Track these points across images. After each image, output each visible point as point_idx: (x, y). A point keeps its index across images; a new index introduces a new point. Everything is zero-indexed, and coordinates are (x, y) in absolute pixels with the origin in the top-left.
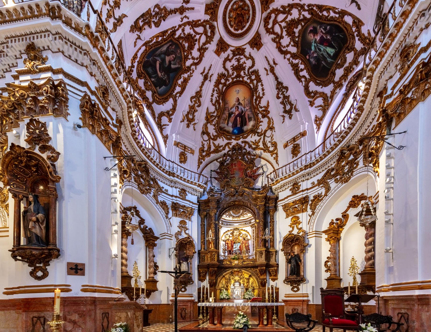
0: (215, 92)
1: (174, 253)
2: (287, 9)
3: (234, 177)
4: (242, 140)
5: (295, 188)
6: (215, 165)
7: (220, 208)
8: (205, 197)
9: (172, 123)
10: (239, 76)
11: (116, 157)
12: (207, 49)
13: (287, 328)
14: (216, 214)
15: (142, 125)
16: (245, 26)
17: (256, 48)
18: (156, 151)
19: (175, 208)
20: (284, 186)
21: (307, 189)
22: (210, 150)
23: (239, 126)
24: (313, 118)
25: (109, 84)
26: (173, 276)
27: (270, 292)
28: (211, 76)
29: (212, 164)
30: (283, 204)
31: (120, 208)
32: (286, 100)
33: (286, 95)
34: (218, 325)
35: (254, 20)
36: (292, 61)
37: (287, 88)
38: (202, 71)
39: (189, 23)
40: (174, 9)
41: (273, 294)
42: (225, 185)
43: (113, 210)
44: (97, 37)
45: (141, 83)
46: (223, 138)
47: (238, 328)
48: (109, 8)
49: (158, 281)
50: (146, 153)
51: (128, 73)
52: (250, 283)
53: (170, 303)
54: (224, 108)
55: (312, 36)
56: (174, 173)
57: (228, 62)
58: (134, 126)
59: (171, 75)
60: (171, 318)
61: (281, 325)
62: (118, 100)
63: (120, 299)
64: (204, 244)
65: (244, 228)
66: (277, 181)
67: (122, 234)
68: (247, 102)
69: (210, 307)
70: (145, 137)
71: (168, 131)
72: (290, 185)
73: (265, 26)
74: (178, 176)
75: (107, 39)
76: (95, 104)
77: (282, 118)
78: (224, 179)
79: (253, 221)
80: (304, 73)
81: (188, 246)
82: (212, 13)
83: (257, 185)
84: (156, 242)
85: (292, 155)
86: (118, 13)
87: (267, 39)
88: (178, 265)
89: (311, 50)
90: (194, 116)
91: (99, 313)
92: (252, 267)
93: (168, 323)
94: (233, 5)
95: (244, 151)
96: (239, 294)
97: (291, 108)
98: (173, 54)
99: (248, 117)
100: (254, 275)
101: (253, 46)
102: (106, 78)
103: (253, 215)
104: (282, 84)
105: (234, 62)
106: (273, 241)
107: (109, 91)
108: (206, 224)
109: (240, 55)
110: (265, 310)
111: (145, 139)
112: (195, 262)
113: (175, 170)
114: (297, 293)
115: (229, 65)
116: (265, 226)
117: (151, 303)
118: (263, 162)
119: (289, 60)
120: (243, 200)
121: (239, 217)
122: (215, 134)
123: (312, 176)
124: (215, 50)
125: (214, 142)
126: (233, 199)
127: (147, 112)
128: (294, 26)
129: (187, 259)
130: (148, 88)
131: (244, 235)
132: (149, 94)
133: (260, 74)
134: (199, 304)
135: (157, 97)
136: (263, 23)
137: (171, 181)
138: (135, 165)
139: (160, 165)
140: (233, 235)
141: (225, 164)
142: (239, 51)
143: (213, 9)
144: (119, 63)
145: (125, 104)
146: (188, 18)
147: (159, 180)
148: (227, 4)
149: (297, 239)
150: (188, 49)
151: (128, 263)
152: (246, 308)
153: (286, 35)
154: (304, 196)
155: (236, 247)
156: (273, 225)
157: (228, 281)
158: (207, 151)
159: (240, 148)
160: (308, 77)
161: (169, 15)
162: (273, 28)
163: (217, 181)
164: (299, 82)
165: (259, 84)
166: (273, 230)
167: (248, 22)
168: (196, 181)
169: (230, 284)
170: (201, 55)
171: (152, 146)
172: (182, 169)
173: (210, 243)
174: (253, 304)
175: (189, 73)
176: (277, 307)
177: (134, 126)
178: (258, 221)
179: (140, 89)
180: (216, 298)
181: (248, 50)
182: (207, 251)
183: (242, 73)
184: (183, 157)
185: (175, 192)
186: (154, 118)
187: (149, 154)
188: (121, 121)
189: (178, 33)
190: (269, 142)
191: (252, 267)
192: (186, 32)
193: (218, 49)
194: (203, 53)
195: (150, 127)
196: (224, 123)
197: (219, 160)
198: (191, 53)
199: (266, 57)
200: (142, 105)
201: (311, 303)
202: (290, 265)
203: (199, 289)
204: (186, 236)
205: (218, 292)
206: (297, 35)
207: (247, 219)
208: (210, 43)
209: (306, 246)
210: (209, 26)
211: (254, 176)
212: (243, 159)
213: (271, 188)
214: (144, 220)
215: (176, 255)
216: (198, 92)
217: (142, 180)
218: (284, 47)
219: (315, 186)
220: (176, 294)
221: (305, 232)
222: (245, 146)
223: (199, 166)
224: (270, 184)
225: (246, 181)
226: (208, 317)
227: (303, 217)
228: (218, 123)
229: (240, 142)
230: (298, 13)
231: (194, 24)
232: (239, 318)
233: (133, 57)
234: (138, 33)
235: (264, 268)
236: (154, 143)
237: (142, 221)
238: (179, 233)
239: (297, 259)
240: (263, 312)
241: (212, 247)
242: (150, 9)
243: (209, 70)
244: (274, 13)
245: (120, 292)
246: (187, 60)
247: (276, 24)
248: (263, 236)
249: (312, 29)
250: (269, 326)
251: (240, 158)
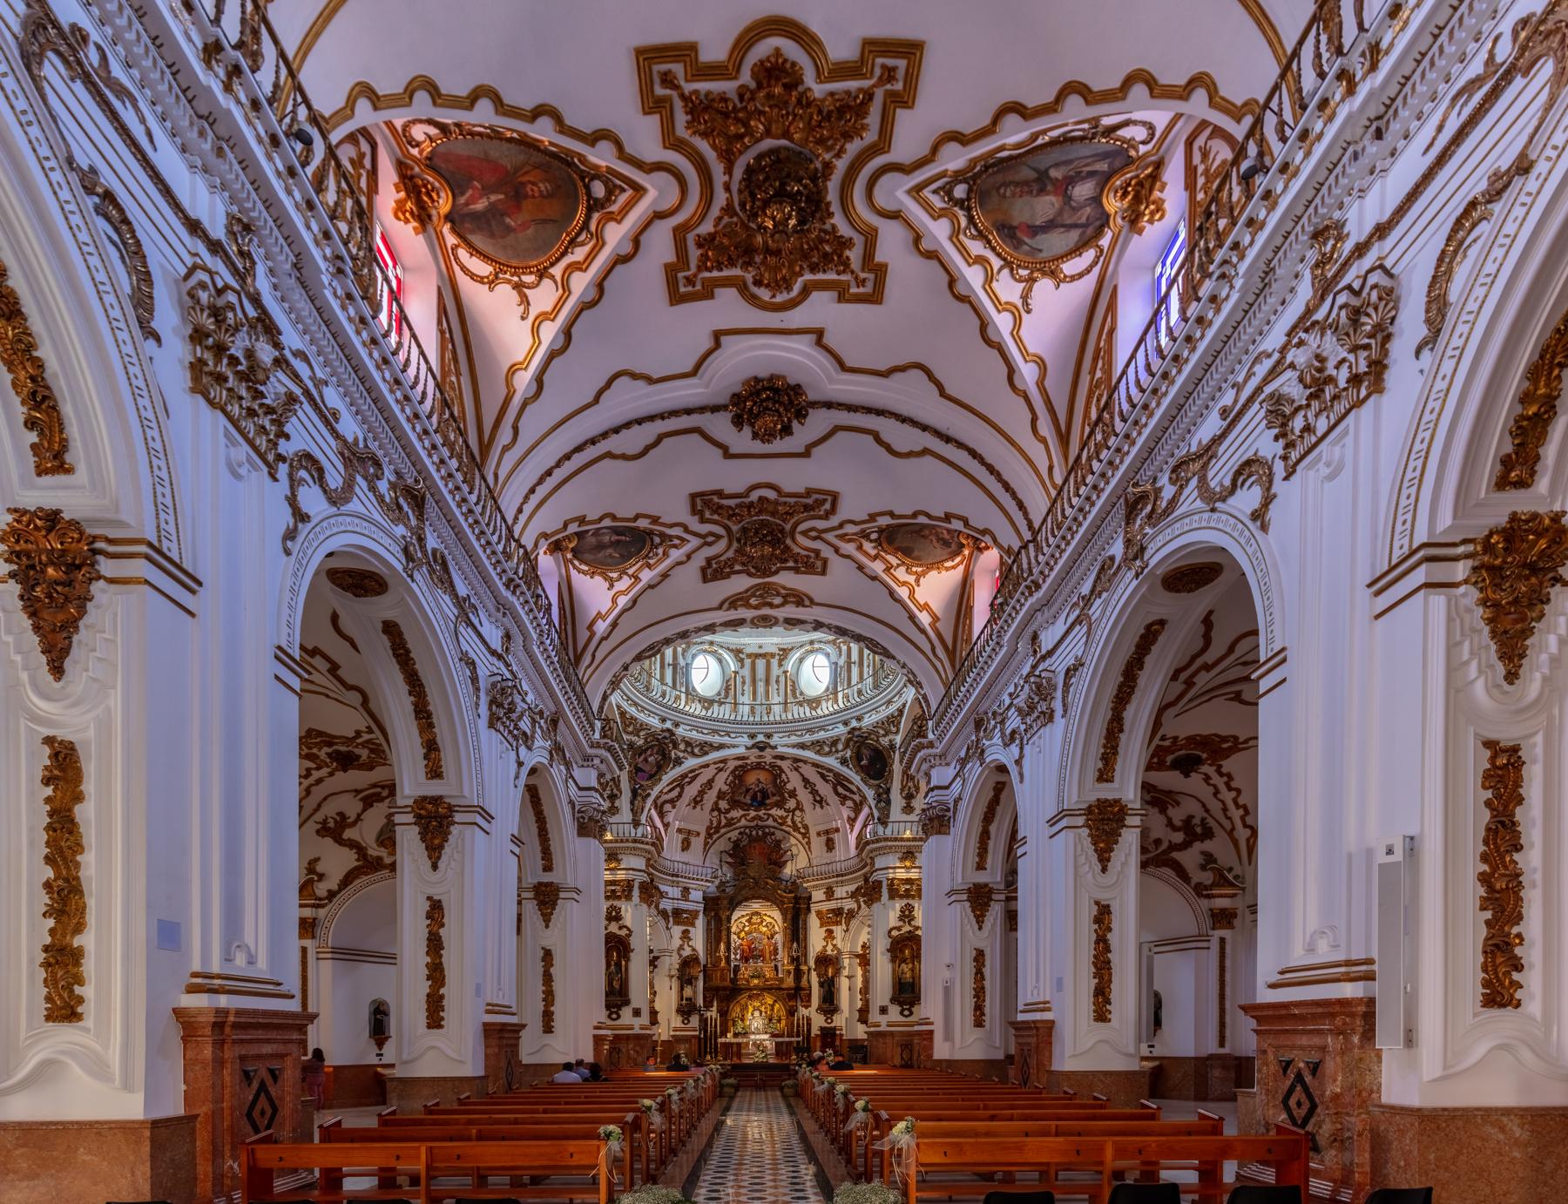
5: (830, 893)
71: (670, 818)
92: (774, 989)
118: (793, 841)
185: (674, 892)
191: (774, 989)
227: (838, 931)
238: (681, 948)
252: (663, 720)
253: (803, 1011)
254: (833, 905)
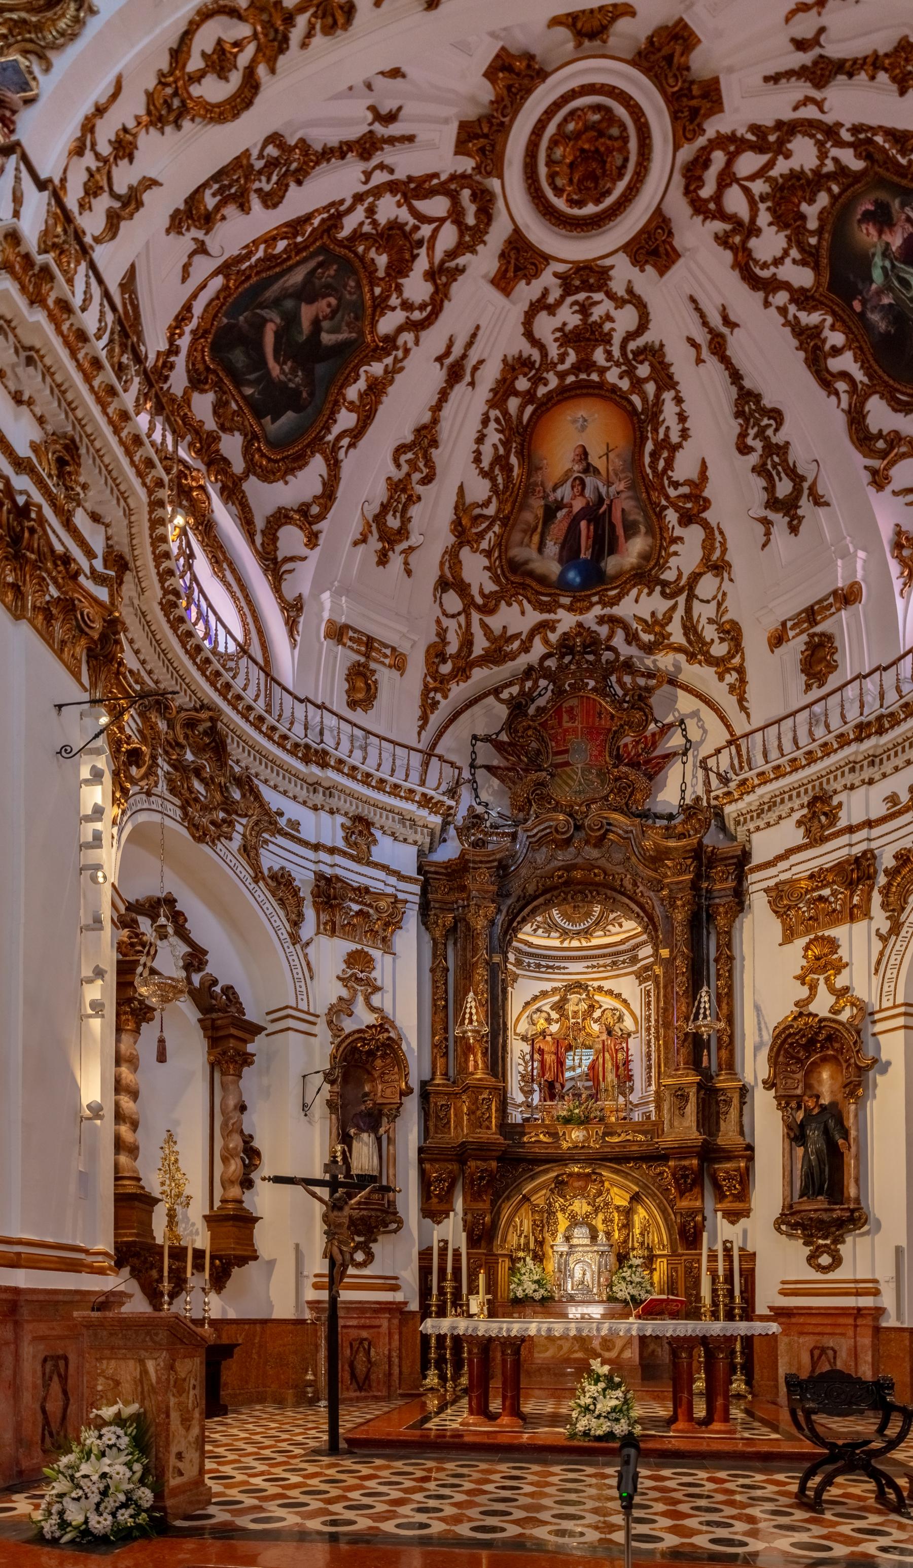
0: (493, 425)
1: (321, 1093)
2: (772, 138)
3: (567, 764)
4: (597, 610)
5: (820, 815)
6: (491, 716)
7: (508, 895)
8: (449, 851)
9: (318, 549)
10: (585, 364)
11: (100, 701)
12: (461, 270)
13: (790, 1438)
14: (492, 923)
15: (202, 566)
16: (609, 192)
17: (655, 266)
18: (256, 663)
19: (328, 897)
20: (772, 805)
21: (869, 824)
22: (470, 652)
23: (585, 555)
24: (886, 533)
25: (83, 427)
26: (320, 1200)
27: (721, 1272)
28: (475, 369)
29: (476, 709)
30: (771, 883)
31: (114, 905)
32: (776, 459)
33: (774, 440)
34: (505, 1420)
35: (646, 169)
36: (795, 317)
37: (777, 415)
38: (441, 350)
39: (392, 187)
40: (336, 145)
41: (729, 1278)
42: (531, 799)
43: (85, 919)
44: (45, 270)
45: (203, 406)
46: (520, 603)
47: (586, 1434)
48: (94, 164)
49: (257, 1219)
50: (218, 674)
51: (155, 378)
52: (637, 1231)
53: (308, 1315)
54: (527, 486)
55: (873, 231)
56: (325, 753)
57: (543, 316)
58: (170, 573)
59: (321, 369)
60: (310, 1384)
61: (765, 1423)
62: (114, 480)
63: (108, 1301)
64: (446, 1054)
65: (607, 985)
66: (743, 782)
67: (118, 1015)
68: (618, 463)
69: (472, 1339)
70: (215, 613)
71: (301, 581)
72: (796, 803)
73: (687, 192)
74: (341, 762)
75: (83, 267)
76: (28, 504)
77: (761, 529)
78: (526, 770)
79: (647, 950)
80: (846, 362)
81: (379, 1063)
82: (482, 150)
83: (661, 797)
84: (250, 1048)
85: (804, 677)
86: (124, 177)
87: (695, 236)
88: (339, 1148)
89: (872, 281)
90: (406, 521)
91: (31, 1354)
92: (636, 1156)
93: (297, 1404)
94: (565, 120)
95: (608, 655)
96: (588, 1277)
97: (797, 492)
98: (330, 295)
99: (624, 520)
100: (653, 1196)
101: (641, 258)
102: (71, 407)
103: (645, 928)
104: (757, 397)
105: (568, 317)
106: (729, 1042)
107: (83, 451)
108: (451, 964)
109: (591, 289)
110: (700, 1354)
111: (212, 619)
112: (409, 1134)
113: (329, 740)
114: (831, 1276)
115: (545, 326)
116: (697, 977)
117: (232, 1315)
118: (686, 703)
119: (783, 311)
120: (602, 862)
121: (587, 933)
122: (490, 587)
123: (888, 767)
124: (492, 275)
125: (488, 620)
126: (564, 857)
127: (223, 516)
128: (800, 193)
129: (374, 1119)
130: (227, 425)
131: (608, 1014)
132: (231, 446)
133: (668, 359)
134: (430, 1326)
135: (263, 455)
136: (678, 180)
137: (314, 786)
138: (171, 726)
139: (271, 720)
140: (563, 1014)
141: (531, 711)
142: (588, 277)
143: (486, 136)
144: (124, 346)
145: (142, 493)
146: (392, 171)
147: (266, 782)
148: (540, 121)
149: (830, 1038)
150: (388, 274)
151: (140, 1138)
152: (619, 1344)
153: (770, 224)
154: (857, 850)
155: (579, 1063)
156: (730, 971)
157: (544, 1221)
158: (458, 656)
159: (593, 644)
160: (859, 376)
161: (317, 163)
162: (718, 197)
163: (496, 782)
164: (824, 393)
165: (668, 396)
166: (730, 994)
167: (620, 176)
168: (412, 783)
169: (554, 1235)
170: (437, 291)
171: (238, 644)
172: (358, 733)
173: (470, 1050)
174: (651, 1327)
175: (389, 360)
176: (748, 1341)
177: (170, 573)
178: (665, 953)
179: (196, 430)
180: (495, 1296)
181: (623, 272)
182: (460, 1086)
183: (599, 356)
184: (360, 684)
185: (327, 829)
186: (250, 535)
187: (227, 676)
188: (121, 557)
189: (349, 224)
190: (710, 621)
191: (636, 1156)
192: (382, 218)
193: (506, 271)
194: (447, 285)
195: (234, 571)
196: (528, 546)
197: (505, 695)
198: (399, 289)
199: (693, 300)
200: (202, 488)
201: (890, 1322)
202: (800, 1151)
203: (425, 1255)
204: (370, 1019)
205: (503, 1266)
206: (812, 224)
207: (622, 942)
208: (474, 252)
209: (869, 1068)
210: (472, 200)
211: (647, 762)
212: (603, 690)
213: (719, 814)
214: (205, 953)
215: (329, 1103)
216: (424, 427)
217: (197, 785)
218: (765, 266)
219: (900, 813)
220: (335, 1278)
221: (860, 1006)
222: (610, 637)
223: (424, 719)
224: (716, 798)
225: (617, 779)
226: (464, 1381)
227: (856, 940)
228: (502, 543)
229: (589, 619)
230: (814, 151)
231: (412, 189)
232: (593, 1389)
233: (177, 317)
234: (200, 235)
235: (695, 1162)
236: (247, 633)
237: (196, 958)
238: (343, 1007)
239: (831, 1123)
240: (690, 1365)
241: (476, 1067)
242: (247, 153)
243: (470, 344)
244: (723, 149)
245: (110, 1268)
246: (383, 314)
247: (730, 185)
248: (687, 1019)
249: (871, 207)
250: (716, 1426)
251: (592, 683)
253: (724, 1230)
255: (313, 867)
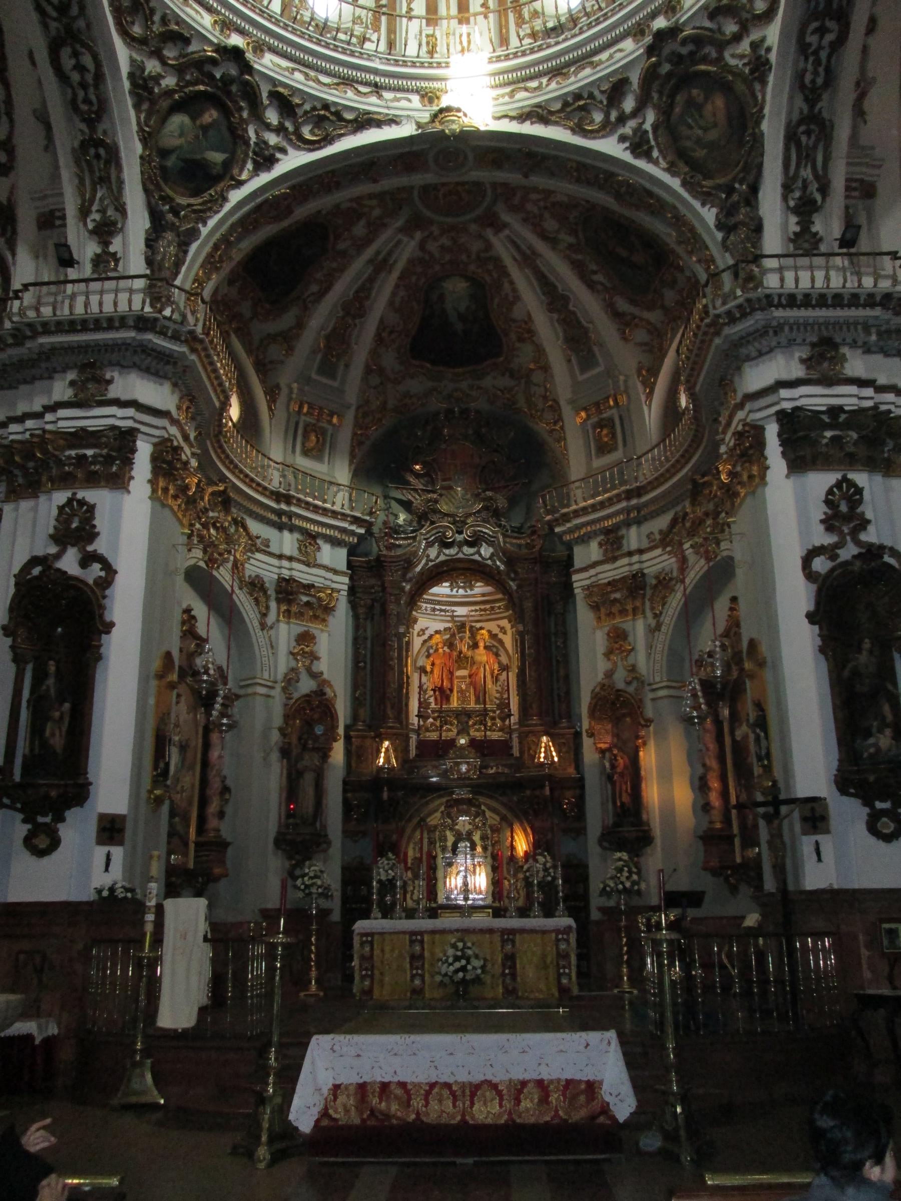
21: (641, 552)
30: (588, 582)
115: (432, 246)
137: (280, 513)
229: (464, 385)
238: (290, 680)
252: (226, 26)
254: (620, 568)
255: (276, 570)
